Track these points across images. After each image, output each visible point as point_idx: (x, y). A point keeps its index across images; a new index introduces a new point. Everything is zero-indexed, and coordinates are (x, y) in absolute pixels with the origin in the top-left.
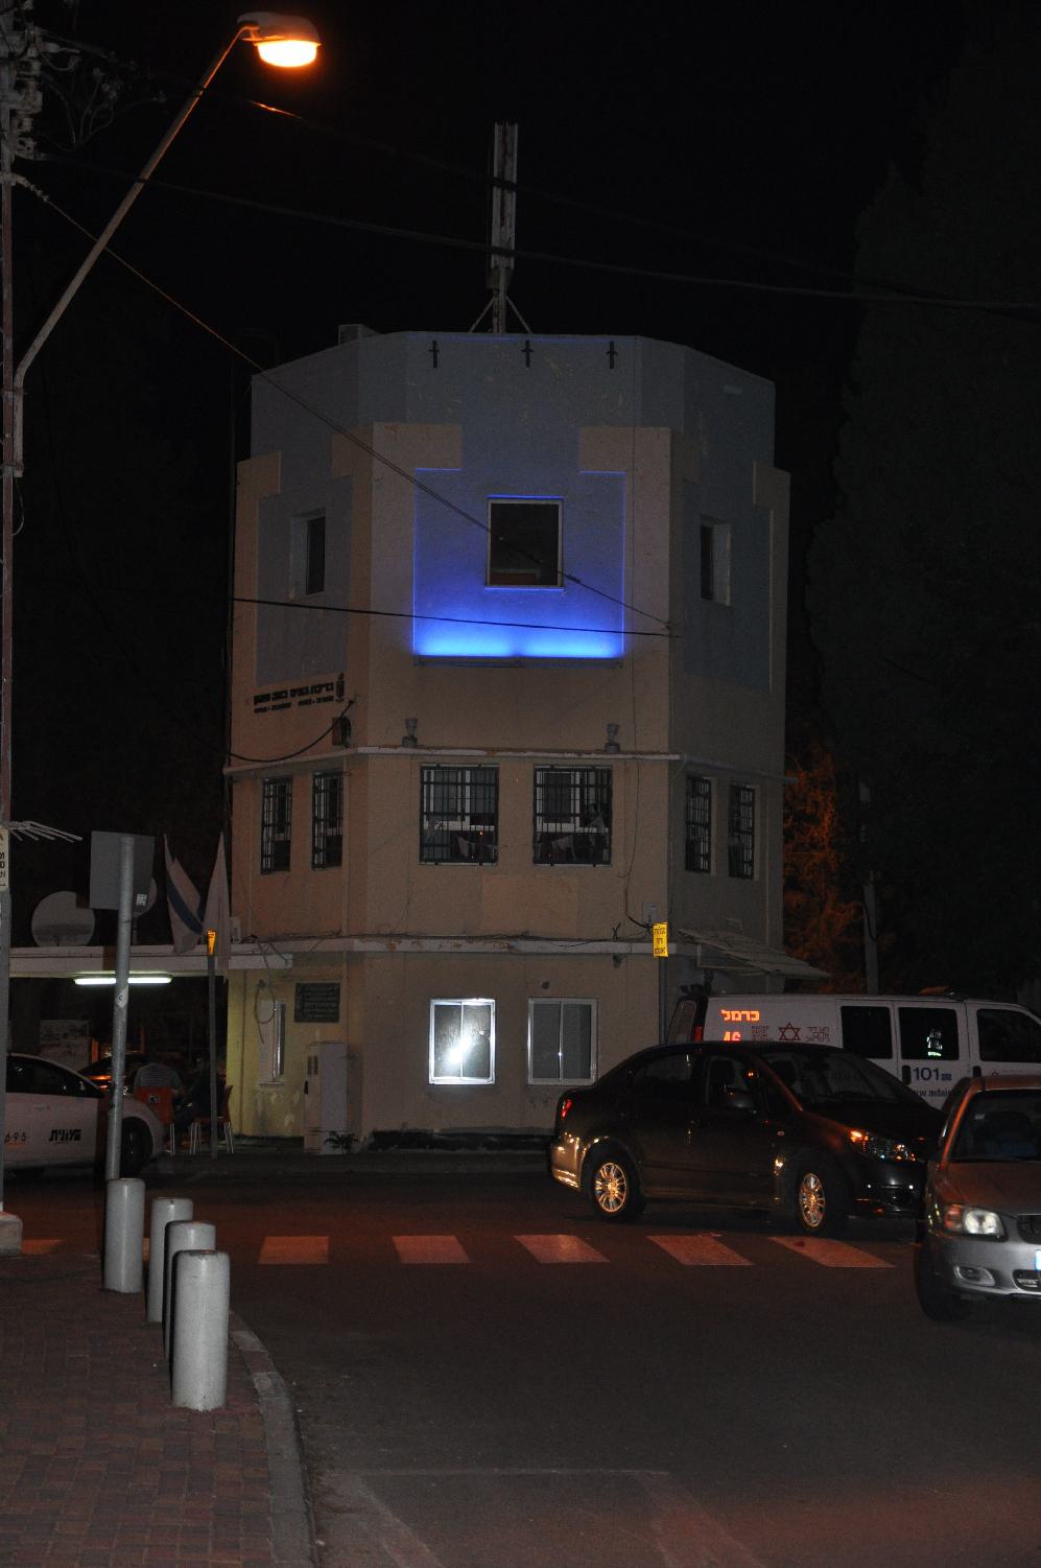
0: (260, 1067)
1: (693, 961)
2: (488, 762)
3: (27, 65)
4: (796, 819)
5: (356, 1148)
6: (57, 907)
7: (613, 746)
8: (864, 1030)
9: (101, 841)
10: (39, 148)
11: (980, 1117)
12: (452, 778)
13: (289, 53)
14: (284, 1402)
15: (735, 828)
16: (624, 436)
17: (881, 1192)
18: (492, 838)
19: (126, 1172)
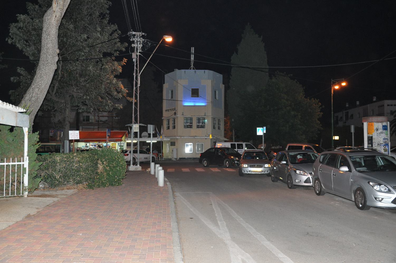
1: (214, 139)
2: (191, 117)
3: (141, 42)
4: (226, 123)
5: (177, 159)
6: (144, 134)
7: (205, 115)
8: (233, 146)
9: (149, 126)
10: (142, 50)
11: (245, 155)
12: (187, 119)
13: (169, 39)
14: (170, 186)
15: (219, 124)
16: (207, 79)
17: (235, 163)
18: (192, 125)
19: (152, 162)
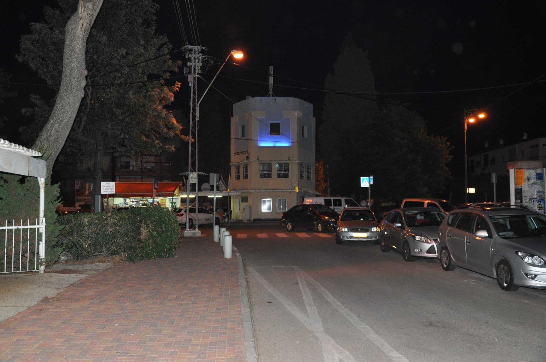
0: (236, 207)
4: (317, 171)
7: (289, 160)
13: (238, 55)
14: (240, 257)
15: (308, 172)
16: (292, 110)
17: (330, 226)
18: (271, 174)
19: (216, 224)
